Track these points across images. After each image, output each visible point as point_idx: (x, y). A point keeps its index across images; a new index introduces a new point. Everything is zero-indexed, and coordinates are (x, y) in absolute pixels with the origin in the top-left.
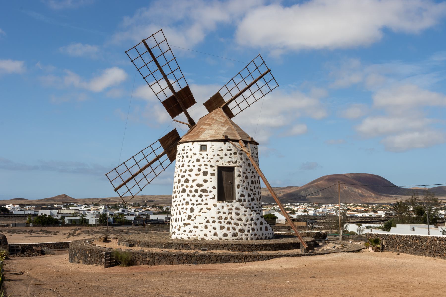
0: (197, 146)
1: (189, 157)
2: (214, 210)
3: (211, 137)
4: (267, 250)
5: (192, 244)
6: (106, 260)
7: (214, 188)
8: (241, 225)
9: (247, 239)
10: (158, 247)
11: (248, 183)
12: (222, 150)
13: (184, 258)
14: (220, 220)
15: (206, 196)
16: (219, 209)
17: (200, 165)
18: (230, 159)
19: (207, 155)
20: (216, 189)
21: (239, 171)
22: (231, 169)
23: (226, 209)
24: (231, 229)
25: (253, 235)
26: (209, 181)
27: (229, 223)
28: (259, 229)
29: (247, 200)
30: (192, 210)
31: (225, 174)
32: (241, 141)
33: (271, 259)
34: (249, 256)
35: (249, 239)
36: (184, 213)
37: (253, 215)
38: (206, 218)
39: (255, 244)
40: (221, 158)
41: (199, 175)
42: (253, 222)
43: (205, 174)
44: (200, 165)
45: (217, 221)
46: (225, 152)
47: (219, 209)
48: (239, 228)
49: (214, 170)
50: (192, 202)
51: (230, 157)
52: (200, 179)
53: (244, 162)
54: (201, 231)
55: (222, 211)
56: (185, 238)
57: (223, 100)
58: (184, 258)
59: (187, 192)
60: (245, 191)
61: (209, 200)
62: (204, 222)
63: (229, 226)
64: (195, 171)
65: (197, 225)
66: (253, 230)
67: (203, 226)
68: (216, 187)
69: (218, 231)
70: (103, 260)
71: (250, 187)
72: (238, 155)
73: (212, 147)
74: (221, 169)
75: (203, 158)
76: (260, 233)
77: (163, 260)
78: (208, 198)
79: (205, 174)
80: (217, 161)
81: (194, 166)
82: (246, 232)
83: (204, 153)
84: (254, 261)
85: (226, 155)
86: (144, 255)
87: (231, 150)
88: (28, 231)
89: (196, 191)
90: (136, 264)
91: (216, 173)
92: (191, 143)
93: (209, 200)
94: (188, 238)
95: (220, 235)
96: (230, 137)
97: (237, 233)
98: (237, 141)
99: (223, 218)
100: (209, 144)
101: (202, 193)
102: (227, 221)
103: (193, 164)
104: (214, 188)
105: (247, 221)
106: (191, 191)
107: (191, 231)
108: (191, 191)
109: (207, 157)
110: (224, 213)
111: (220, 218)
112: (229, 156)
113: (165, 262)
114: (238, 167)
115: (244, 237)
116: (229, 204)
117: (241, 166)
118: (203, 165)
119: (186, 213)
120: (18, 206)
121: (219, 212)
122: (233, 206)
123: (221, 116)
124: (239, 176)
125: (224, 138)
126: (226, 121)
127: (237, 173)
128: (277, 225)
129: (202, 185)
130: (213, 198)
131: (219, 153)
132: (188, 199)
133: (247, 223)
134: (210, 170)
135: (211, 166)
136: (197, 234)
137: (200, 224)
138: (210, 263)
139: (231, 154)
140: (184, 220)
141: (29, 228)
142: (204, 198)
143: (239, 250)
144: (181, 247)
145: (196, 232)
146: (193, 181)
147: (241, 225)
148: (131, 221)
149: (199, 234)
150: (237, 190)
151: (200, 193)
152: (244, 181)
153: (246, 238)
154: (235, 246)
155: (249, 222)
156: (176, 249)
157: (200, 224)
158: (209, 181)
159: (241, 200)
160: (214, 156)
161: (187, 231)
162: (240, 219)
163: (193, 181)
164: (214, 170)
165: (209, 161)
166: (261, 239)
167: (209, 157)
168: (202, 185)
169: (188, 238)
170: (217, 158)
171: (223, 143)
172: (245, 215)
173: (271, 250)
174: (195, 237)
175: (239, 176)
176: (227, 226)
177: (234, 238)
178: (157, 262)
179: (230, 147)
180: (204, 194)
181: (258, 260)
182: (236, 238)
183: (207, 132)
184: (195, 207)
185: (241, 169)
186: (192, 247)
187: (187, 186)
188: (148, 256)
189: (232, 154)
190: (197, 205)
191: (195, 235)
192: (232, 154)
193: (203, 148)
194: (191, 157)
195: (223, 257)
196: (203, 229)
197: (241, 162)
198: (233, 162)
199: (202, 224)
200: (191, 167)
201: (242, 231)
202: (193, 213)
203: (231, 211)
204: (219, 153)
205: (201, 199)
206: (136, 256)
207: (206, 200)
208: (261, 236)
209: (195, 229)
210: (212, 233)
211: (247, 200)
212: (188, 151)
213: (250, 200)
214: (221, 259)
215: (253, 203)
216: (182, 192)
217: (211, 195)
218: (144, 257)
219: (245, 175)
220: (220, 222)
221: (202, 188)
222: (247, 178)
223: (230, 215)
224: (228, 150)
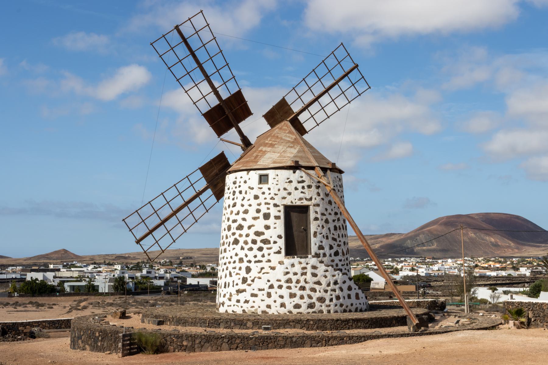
0: (254, 176)
1: (243, 192)
2: (280, 269)
3: (274, 162)
4: (359, 328)
5: (249, 320)
6: (123, 345)
7: (280, 237)
8: (320, 291)
9: (329, 312)
10: (199, 325)
11: (329, 229)
12: (291, 182)
13: (238, 341)
15: (268, 249)
16: (287, 268)
17: (259, 205)
21: (316, 212)
22: (304, 210)
23: (298, 269)
25: (338, 305)
27: (303, 288)
28: (346, 297)
29: (328, 255)
30: (248, 270)
32: (318, 169)
33: (365, 340)
34: (332, 337)
35: (332, 312)
36: (237, 274)
37: (337, 276)
38: (269, 281)
40: (290, 194)
41: (258, 218)
42: (338, 286)
43: (267, 216)
44: (259, 205)
45: (285, 285)
46: (295, 184)
47: (287, 268)
48: (317, 296)
49: (279, 211)
50: (248, 259)
51: (302, 192)
53: (323, 199)
54: (262, 300)
55: (292, 270)
56: (239, 311)
57: (291, 109)
58: (238, 341)
59: (241, 243)
60: (324, 241)
61: (272, 254)
62: (266, 287)
63: (302, 292)
64: (252, 213)
65: (256, 292)
66: (338, 298)
67: (264, 293)
68: (283, 235)
70: (120, 345)
72: (314, 188)
73: (276, 177)
74: (289, 210)
75: (263, 193)
76: (348, 302)
77: (207, 345)
79: (267, 216)
80: (284, 198)
81: (250, 205)
82: (327, 302)
83: (265, 187)
85: (296, 189)
86: (180, 337)
87: (303, 181)
88: (11, 303)
89: (254, 242)
90: (167, 351)
92: (246, 172)
93: (272, 254)
94: (244, 311)
95: (290, 307)
96: (302, 163)
97: (314, 303)
98: (313, 168)
99: (294, 280)
101: (262, 245)
103: (249, 203)
104: (280, 237)
106: (246, 243)
107: (247, 302)
108: (246, 243)
109: (269, 192)
110: (295, 274)
111: (289, 281)
112: (300, 190)
113: (210, 348)
114: (314, 205)
116: (303, 260)
117: (318, 205)
119: (239, 274)
121: (287, 273)
122: (307, 264)
124: (316, 219)
125: (293, 164)
126: (295, 139)
127: (312, 215)
128: (373, 291)
129: (263, 234)
130: (279, 252)
132: (242, 254)
133: (329, 288)
134: (273, 212)
135: (276, 205)
137: (260, 290)
138: (275, 347)
139: (303, 187)
140: (237, 284)
141: (13, 298)
142: (265, 251)
144: (232, 324)
145: (254, 302)
146: (249, 227)
147: (320, 291)
148: (160, 287)
149: (258, 305)
150: (313, 240)
151: (259, 244)
152: (323, 227)
153: (328, 310)
156: (226, 328)
157: (260, 290)
158: (272, 226)
159: (320, 254)
160: (279, 190)
161: (242, 301)
162: (319, 283)
163: (249, 227)
164: (279, 211)
165: (272, 198)
166: (350, 311)
168: (263, 234)
169: (244, 311)
170: (284, 193)
171: (292, 171)
173: (365, 328)
174: (253, 309)
175: (316, 219)
176: (299, 293)
177: (310, 310)
178: (198, 347)
179: (302, 177)
180: (265, 246)
181: (346, 343)
182: (313, 310)
183: (268, 155)
185: (318, 209)
186: (249, 324)
187: (241, 235)
188: (184, 338)
189: (306, 187)
190: (256, 262)
191: (252, 307)
192: (306, 187)
193: (263, 179)
194: (246, 193)
195: (294, 339)
196: (265, 297)
198: (306, 199)
199: (264, 290)
200: (246, 207)
201: (321, 300)
202: (250, 274)
203: (305, 271)
206: (168, 338)
207: (269, 255)
208: (350, 307)
211: (328, 255)
212: (242, 184)
213: (333, 255)
215: (337, 259)
216: (233, 244)
217: (276, 248)
218: (180, 340)
219: (324, 218)
220: (289, 288)
221: (262, 237)
223: (304, 277)
224: (299, 182)
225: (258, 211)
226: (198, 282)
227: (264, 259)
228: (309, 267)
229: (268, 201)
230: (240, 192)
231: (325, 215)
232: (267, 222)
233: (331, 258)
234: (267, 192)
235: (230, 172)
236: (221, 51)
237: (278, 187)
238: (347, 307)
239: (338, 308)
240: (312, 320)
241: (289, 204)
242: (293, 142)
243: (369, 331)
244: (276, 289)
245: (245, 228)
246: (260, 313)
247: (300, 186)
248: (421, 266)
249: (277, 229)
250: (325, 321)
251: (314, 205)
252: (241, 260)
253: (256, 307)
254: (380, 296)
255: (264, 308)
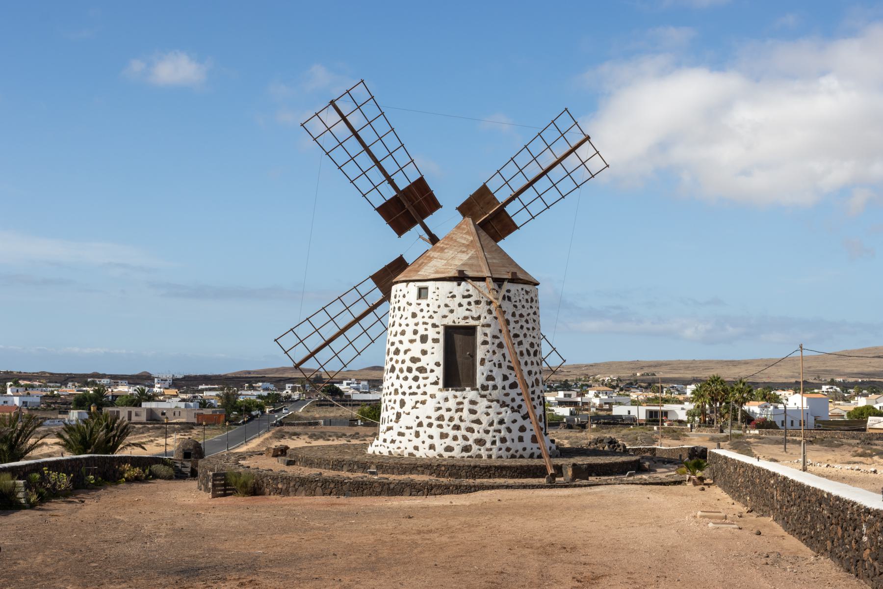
1: (402, 309)
2: (431, 404)
3: (437, 272)
4: (504, 477)
6: (214, 485)
7: (437, 364)
8: (478, 432)
9: (490, 457)
11: (504, 355)
13: (332, 486)
14: (441, 423)
15: (424, 378)
17: (417, 324)
18: (467, 313)
19: (428, 305)
20: (442, 366)
21: (486, 335)
22: (470, 331)
23: (452, 404)
24: (460, 438)
25: (504, 449)
26: (429, 353)
27: (457, 428)
28: (516, 440)
29: (500, 387)
30: (403, 403)
31: (458, 342)
32: (489, 280)
33: (475, 491)
34: (435, 485)
35: (493, 457)
36: (393, 408)
37: (504, 414)
38: (417, 418)
39: (479, 466)
40: (452, 311)
41: (415, 341)
42: (504, 426)
43: (424, 339)
44: (417, 324)
45: (436, 423)
46: (459, 299)
48: (475, 437)
49: (438, 333)
51: (467, 310)
52: (416, 349)
53: (496, 318)
55: (445, 405)
56: (385, 453)
57: (495, 198)
58: (332, 486)
59: (397, 371)
60: (496, 370)
61: (428, 385)
62: (414, 424)
63: (455, 432)
64: (409, 335)
65: (403, 430)
66: (503, 440)
67: (413, 431)
68: (442, 363)
69: (437, 441)
70: (210, 484)
71: (507, 363)
72: (483, 304)
73: (437, 291)
74: (450, 332)
76: (519, 446)
77: (301, 488)
78: (428, 382)
79: (424, 339)
80: (445, 317)
81: (407, 325)
82: (488, 445)
83: (424, 302)
84: (444, 494)
85: (460, 305)
87: (469, 296)
88: (348, 434)
89: (410, 370)
90: (263, 494)
91: (441, 337)
92: (405, 284)
93: (428, 385)
94: (390, 452)
95: (440, 449)
96: (470, 273)
97: (470, 446)
98: (483, 279)
99: (447, 418)
100: (431, 285)
101: (418, 374)
102: (452, 424)
104: (437, 364)
105: (491, 424)
107: (393, 441)
108: (401, 371)
109: (428, 309)
110: (449, 410)
111: (440, 418)
112: (466, 306)
114: (483, 326)
115: (484, 453)
116: (458, 394)
117: (489, 326)
118: (421, 323)
120: (366, 383)
122: (464, 398)
123: (465, 234)
124: (485, 343)
125: (457, 275)
126: (472, 241)
127: (480, 338)
128: (871, 431)
129: (419, 360)
130: (436, 383)
131: (448, 301)
133: (491, 429)
134: (432, 333)
136: (402, 446)
137: (408, 428)
138: (371, 495)
139: (469, 304)
141: (355, 428)
142: (421, 382)
143: (450, 475)
146: (406, 352)
147: (478, 432)
148: (563, 417)
150: (479, 369)
151: (415, 373)
152: (494, 352)
153: (490, 453)
154: (443, 468)
155: (496, 426)
156: (348, 471)
157: (408, 428)
158: (429, 351)
159: (488, 386)
160: (439, 307)
161: (389, 441)
162: (478, 422)
163: (406, 352)
164: (438, 333)
165: (431, 317)
166: (521, 457)
167: (431, 309)
168: (419, 360)
169: (390, 452)
170: (445, 311)
171: (455, 283)
172: (488, 414)
173: (512, 477)
174: (399, 451)
175: (485, 343)
176: (452, 433)
177: (465, 454)
179: (468, 291)
180: (421, 376)
181: (452, 493)
182: (469, 454)
183: (434, 263)
184: (407, 398)
185: (488, 330)
189: (473, 303)
190: (410, 394)
191: (399, 448)
192: (473, 303)
193: (422, 293)
195: (392, 486)
196: (413, 437)
197: (489, 317)
198: (473, 318)
199: (411, 428)
200: (404, 327)
201: (480, 442)
203: (461, 406)
204: (448, 301)
205: (417, 384)
206: (265, 480)
207: (425, 386)
208: (521, 452)
209: (400, 438)
210: (427, 445)
211: (500, 387)
213: (507, 387)
214: (389, 489)
215: (513, 393)
217: (432, 378)
219: (497, 341)
220: (440, 426)
221: (419, 364)
222: (500, 346)
223: (459, 414)
224: (464, 297)
225: (415, 332)
226: (629, 412)
227: (420, 391)
228: (466, 401)
229: (426, 320)
230: (399, 309)
231: (498, 338)
232: (425, 346)
233: (505, 392)
234: (426, 309)
235: (397, 282)
236: (393, 129)
237: (438, 303)
238: (517, 451)
239: (503, 453)
240: (444, 465)
241: (451, 324)
242: (467, 246)
243: (485, 481)
244: (425, 427)
245: (402, 353)
246: (406, 455)
247: (465, 302)
248: (49, 416)
249: (436, 354)
250: (460, 468)
251: (483, 326)
252: (396, 391)
253: (403, 448)
254: (877, 439)
255: (411, 450)
